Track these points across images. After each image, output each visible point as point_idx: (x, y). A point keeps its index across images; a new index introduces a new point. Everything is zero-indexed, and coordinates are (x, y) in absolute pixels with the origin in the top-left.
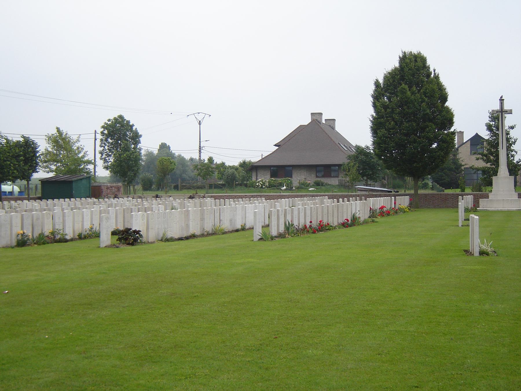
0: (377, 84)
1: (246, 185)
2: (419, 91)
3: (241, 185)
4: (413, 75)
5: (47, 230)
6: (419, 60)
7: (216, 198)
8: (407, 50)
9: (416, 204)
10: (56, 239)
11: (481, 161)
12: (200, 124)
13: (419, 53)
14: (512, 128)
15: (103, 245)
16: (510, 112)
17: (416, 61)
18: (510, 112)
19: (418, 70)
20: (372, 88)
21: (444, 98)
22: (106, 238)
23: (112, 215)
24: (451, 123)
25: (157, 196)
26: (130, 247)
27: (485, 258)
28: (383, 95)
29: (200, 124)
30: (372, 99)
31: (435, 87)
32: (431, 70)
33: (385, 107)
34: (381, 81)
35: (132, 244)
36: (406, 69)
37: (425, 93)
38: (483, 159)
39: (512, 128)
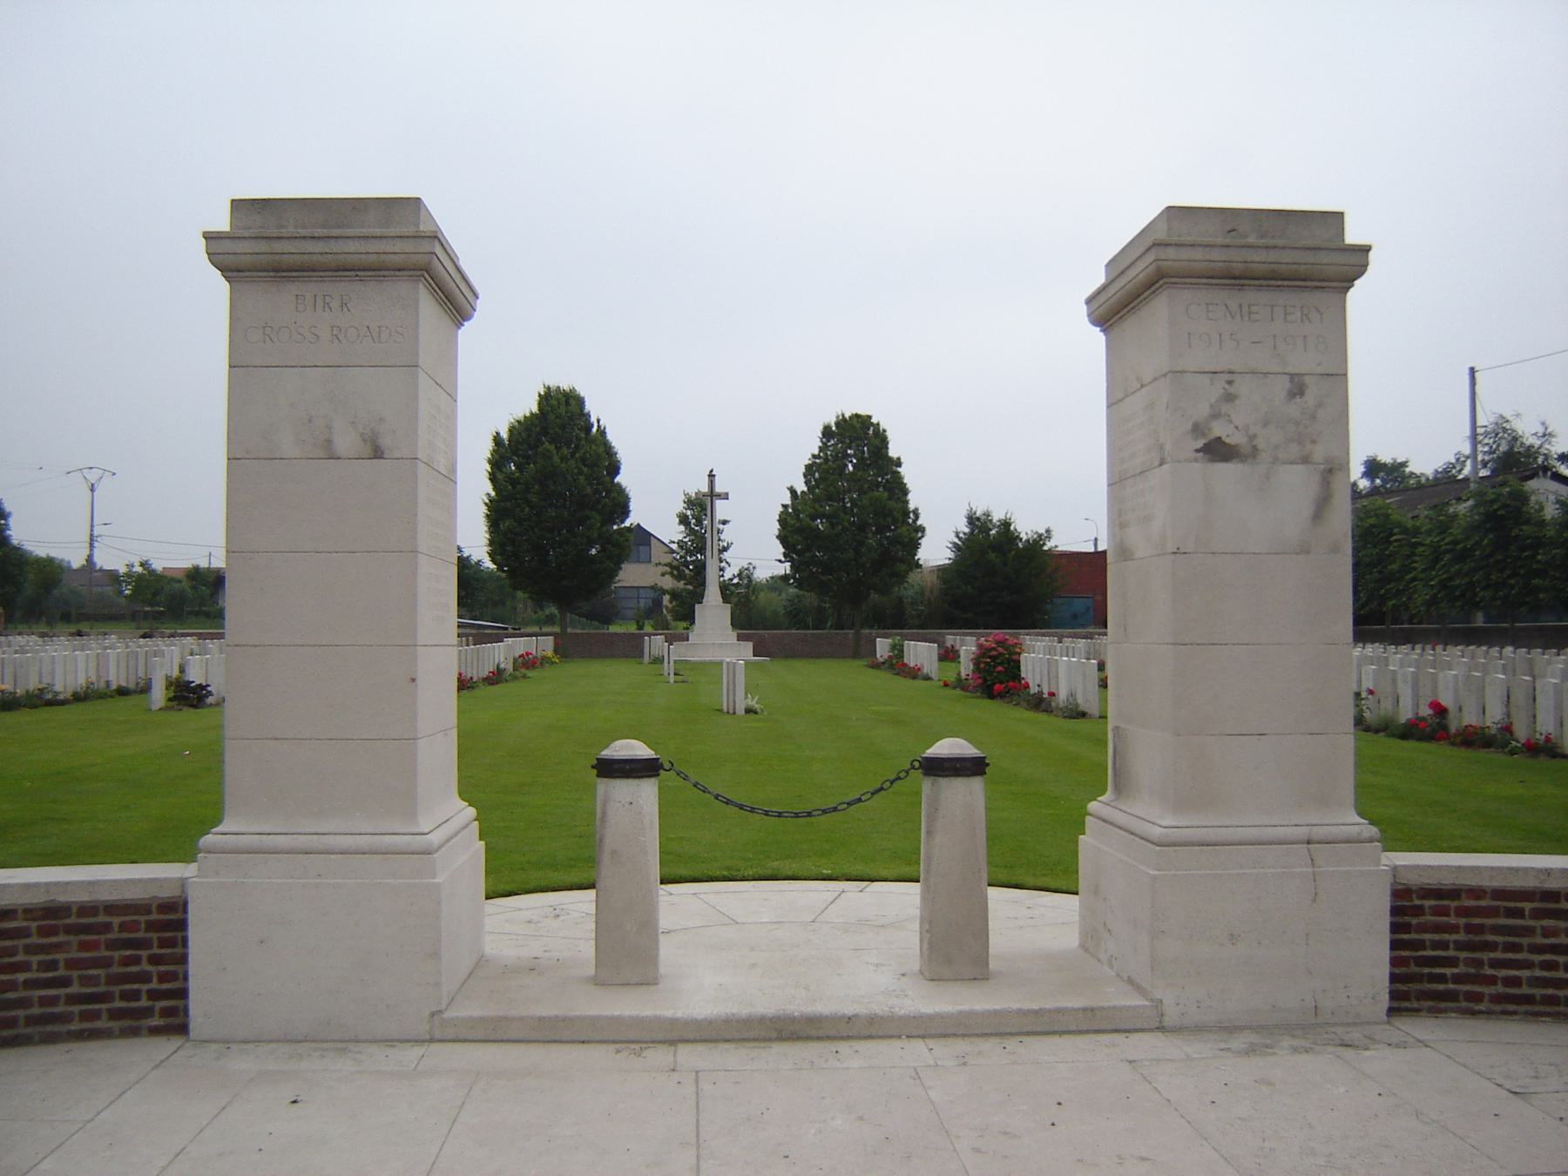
0: (497, 439)
1: (207, 615)
2: (573, 455)
3: (197, 614)
4: (563, 427)
5: (33, 684)
6: (573, 402)
7: (201, 636)
8: (553, 384)
9: (566, 650)
10: (41, 700)
11: (668, 577)
12: (92, 490)
13: (573, 391)
14: (724, 522)
15: (155, 707)
16: (725, 496)
17: (567, 403)
18: (725, 496)
19: (571, 418)
20: (488, 447)
21: (615, 469)
22: (159, 695)
23: (81, 666)
24: (625, 512)
25: (80, 634)
26: (192, 710)
27: (752, 716)
28: (509, 460)
29: (92, 490)
30: (488, 467)
31: (601, 449)
32: (593, 419)
33: (513, 481)
34: (505, 435)
35: (195, 707)
36: (552, 417)
37: (583, 460)
38: (671, 574)
39: (724, 522)
